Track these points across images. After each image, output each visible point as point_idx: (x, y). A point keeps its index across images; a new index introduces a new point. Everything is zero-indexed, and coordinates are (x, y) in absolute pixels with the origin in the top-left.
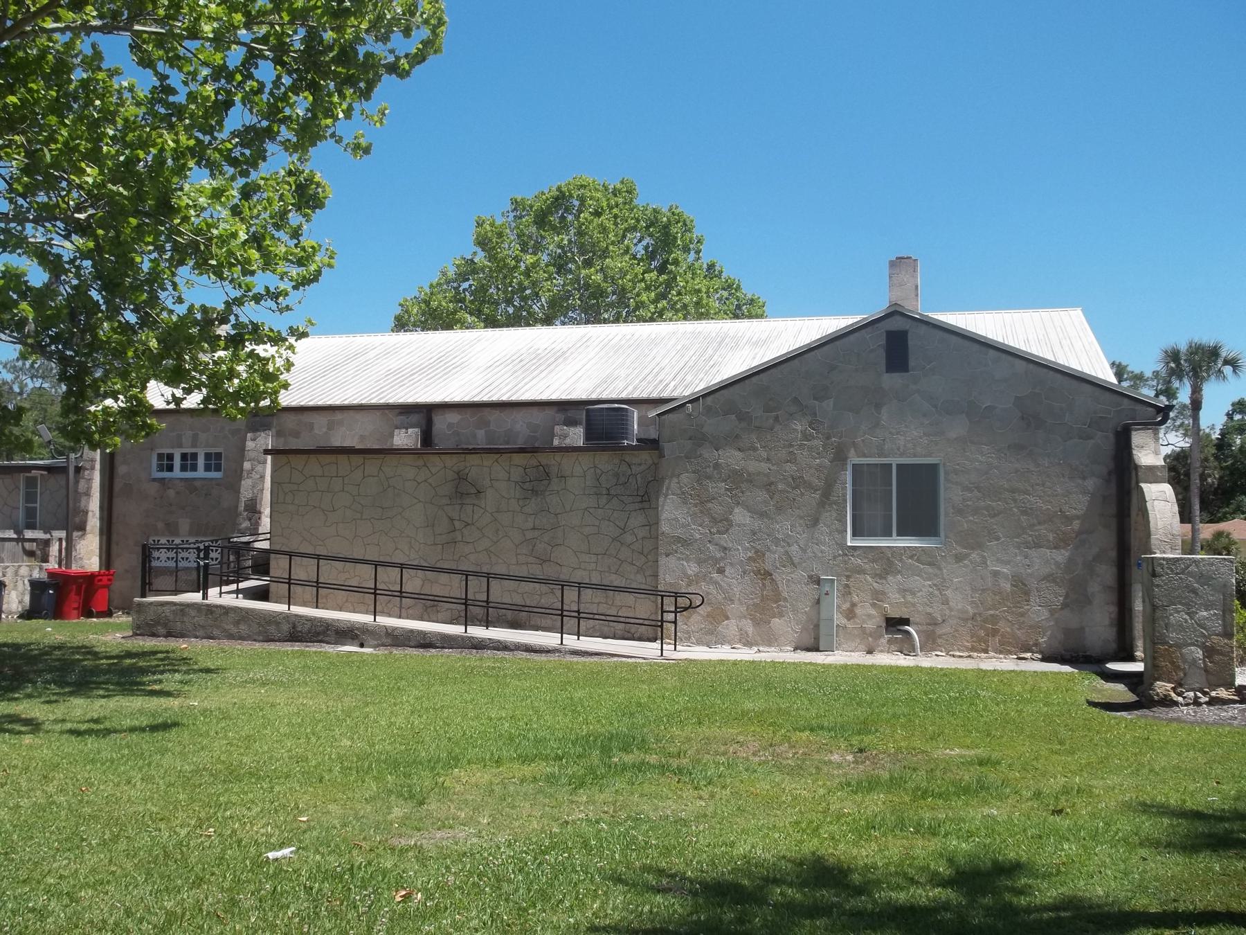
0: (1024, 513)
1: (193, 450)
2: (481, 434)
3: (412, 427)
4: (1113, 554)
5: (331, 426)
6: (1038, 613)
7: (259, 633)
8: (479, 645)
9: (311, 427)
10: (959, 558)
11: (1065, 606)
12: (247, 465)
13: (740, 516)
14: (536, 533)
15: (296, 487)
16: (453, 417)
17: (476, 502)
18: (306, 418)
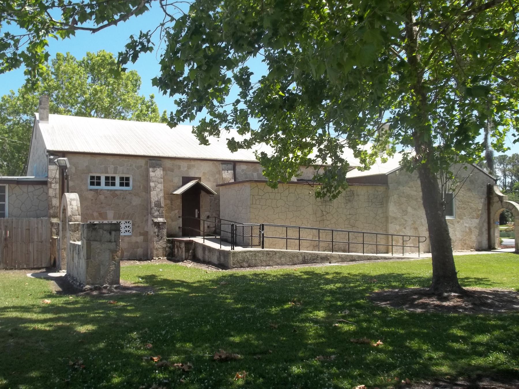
0: (471, 209)
1: (113, 175)
2: (255, 174)
3: (230, 170)
4: (487, 220)
5: (189, 167)
6: (474, 238)
7: (290, 261)
8: (377, 258)
9: (179, 167)
10: (458, 222)
11: (479, 235)
12: (152, 184)
13: (410, 209)
14: (351, 216)
15: (260, 197)
16: (244, 167)
17: (331, 204)
18: (177, 162)
